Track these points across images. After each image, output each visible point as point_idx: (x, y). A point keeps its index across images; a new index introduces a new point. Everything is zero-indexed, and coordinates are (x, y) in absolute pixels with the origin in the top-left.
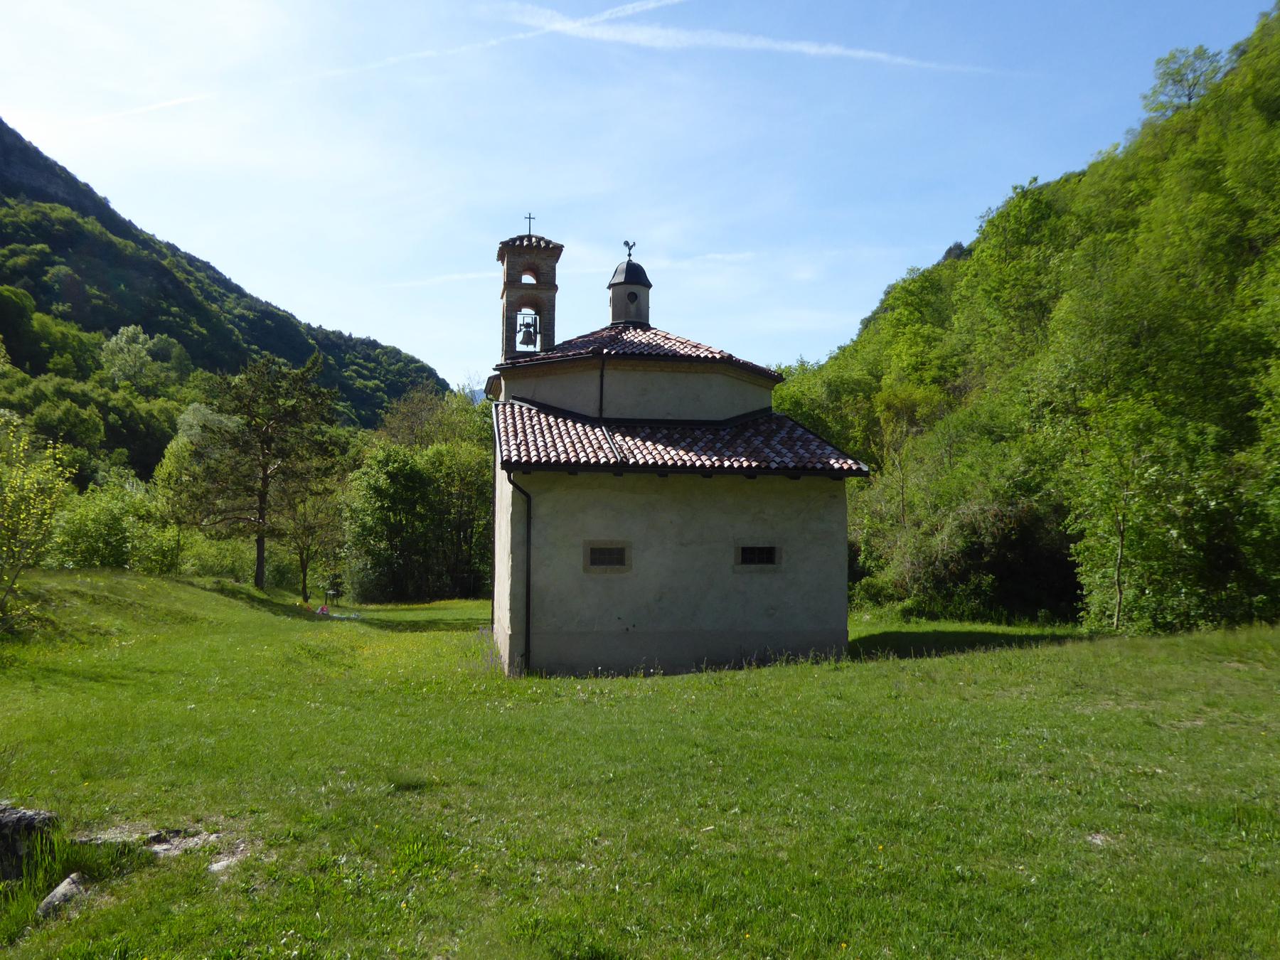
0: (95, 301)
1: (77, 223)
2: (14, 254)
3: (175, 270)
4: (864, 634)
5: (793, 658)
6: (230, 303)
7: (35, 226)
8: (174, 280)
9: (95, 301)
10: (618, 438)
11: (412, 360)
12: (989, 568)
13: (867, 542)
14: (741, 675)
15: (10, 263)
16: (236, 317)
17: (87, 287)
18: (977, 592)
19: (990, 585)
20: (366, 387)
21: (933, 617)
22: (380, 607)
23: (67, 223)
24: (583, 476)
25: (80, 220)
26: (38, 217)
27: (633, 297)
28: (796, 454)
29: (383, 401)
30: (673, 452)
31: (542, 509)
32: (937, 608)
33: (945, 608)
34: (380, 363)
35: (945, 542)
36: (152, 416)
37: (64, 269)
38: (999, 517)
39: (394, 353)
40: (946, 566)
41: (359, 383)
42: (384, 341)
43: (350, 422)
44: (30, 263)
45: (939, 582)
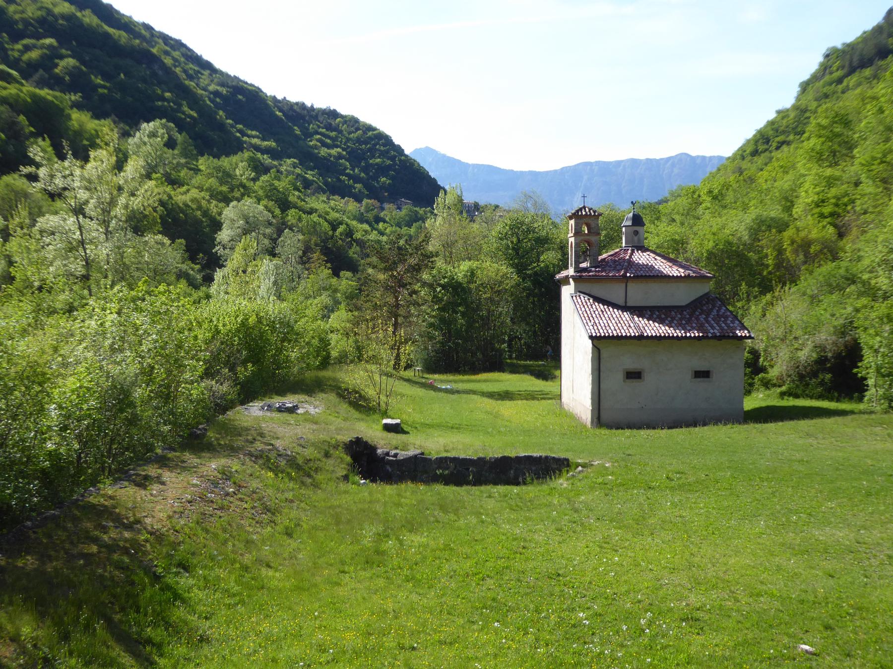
0: (101, 90)
1: (77, 17)
2: (27, 48)
3: (163, 57)
4: (757, 406)
5: (716, 423)
6: (204, 79)
7: (42, 21)
8: (163, 66)
9: (101, 90)
10: (636, 319)
11: (370, 128)
12: (829, 371)
13: (765, 351)
14: (697, 429)
15: (25, 57)
16: (211, 93)
17: (93, 77)
18: (822, 383)
19: (830, 380)
20: (330, 155)
21: (797, 396)
22: (461, 377)
23: (69, 18)
24: (623, 341)
25: (79, 14)
26: (44, 14)
27: (636, 233)
28: (720, 326)
29: (346, 168)
30: (663, 328)
31: (605, 354)
32: (800, 392)
33: (804, 391)
34: (340, 132)
35: (806, 354)
36: (187, 206)
37: (71, 62)
38: (835, 343)
39: (353, 122)
40: (805, 367)
41: (324, 152)
42: (343, 110)
43: (319, 190)
44: (43, 57)
45: (801, 377)
